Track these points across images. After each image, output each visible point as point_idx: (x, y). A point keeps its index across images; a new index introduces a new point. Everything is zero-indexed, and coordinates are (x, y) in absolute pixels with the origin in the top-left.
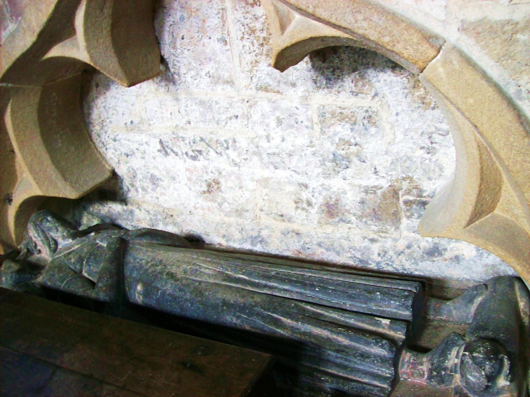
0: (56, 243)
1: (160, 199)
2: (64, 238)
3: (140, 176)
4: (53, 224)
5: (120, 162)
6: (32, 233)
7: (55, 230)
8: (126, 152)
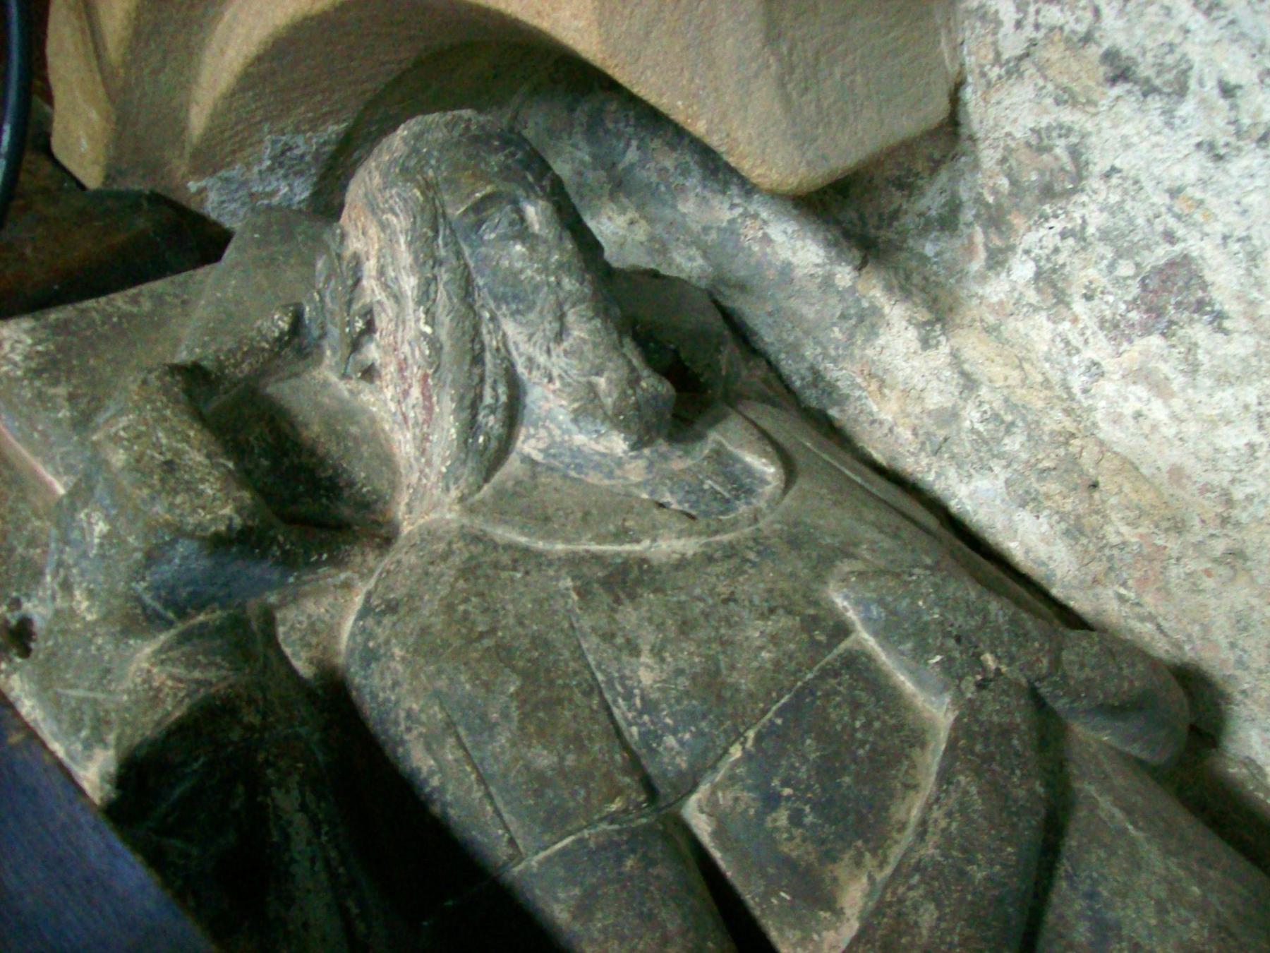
0: (514, 412)
1: (1108, 387)
2: (588, 407)
3: (1090, 210)
4: (545, 270)
5: (1028, 68)
6: (379, 235)
7: (550, 327)
8: (1127, 48)
